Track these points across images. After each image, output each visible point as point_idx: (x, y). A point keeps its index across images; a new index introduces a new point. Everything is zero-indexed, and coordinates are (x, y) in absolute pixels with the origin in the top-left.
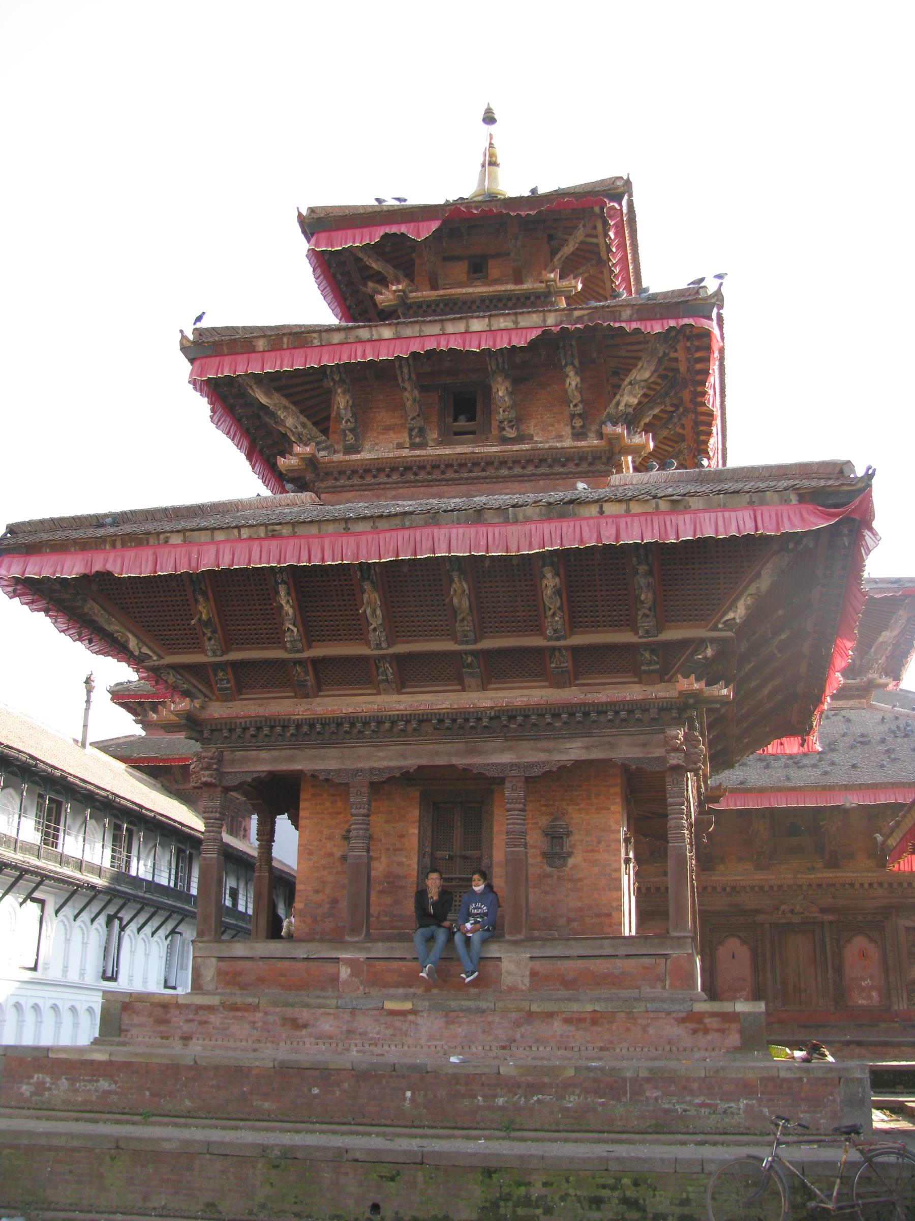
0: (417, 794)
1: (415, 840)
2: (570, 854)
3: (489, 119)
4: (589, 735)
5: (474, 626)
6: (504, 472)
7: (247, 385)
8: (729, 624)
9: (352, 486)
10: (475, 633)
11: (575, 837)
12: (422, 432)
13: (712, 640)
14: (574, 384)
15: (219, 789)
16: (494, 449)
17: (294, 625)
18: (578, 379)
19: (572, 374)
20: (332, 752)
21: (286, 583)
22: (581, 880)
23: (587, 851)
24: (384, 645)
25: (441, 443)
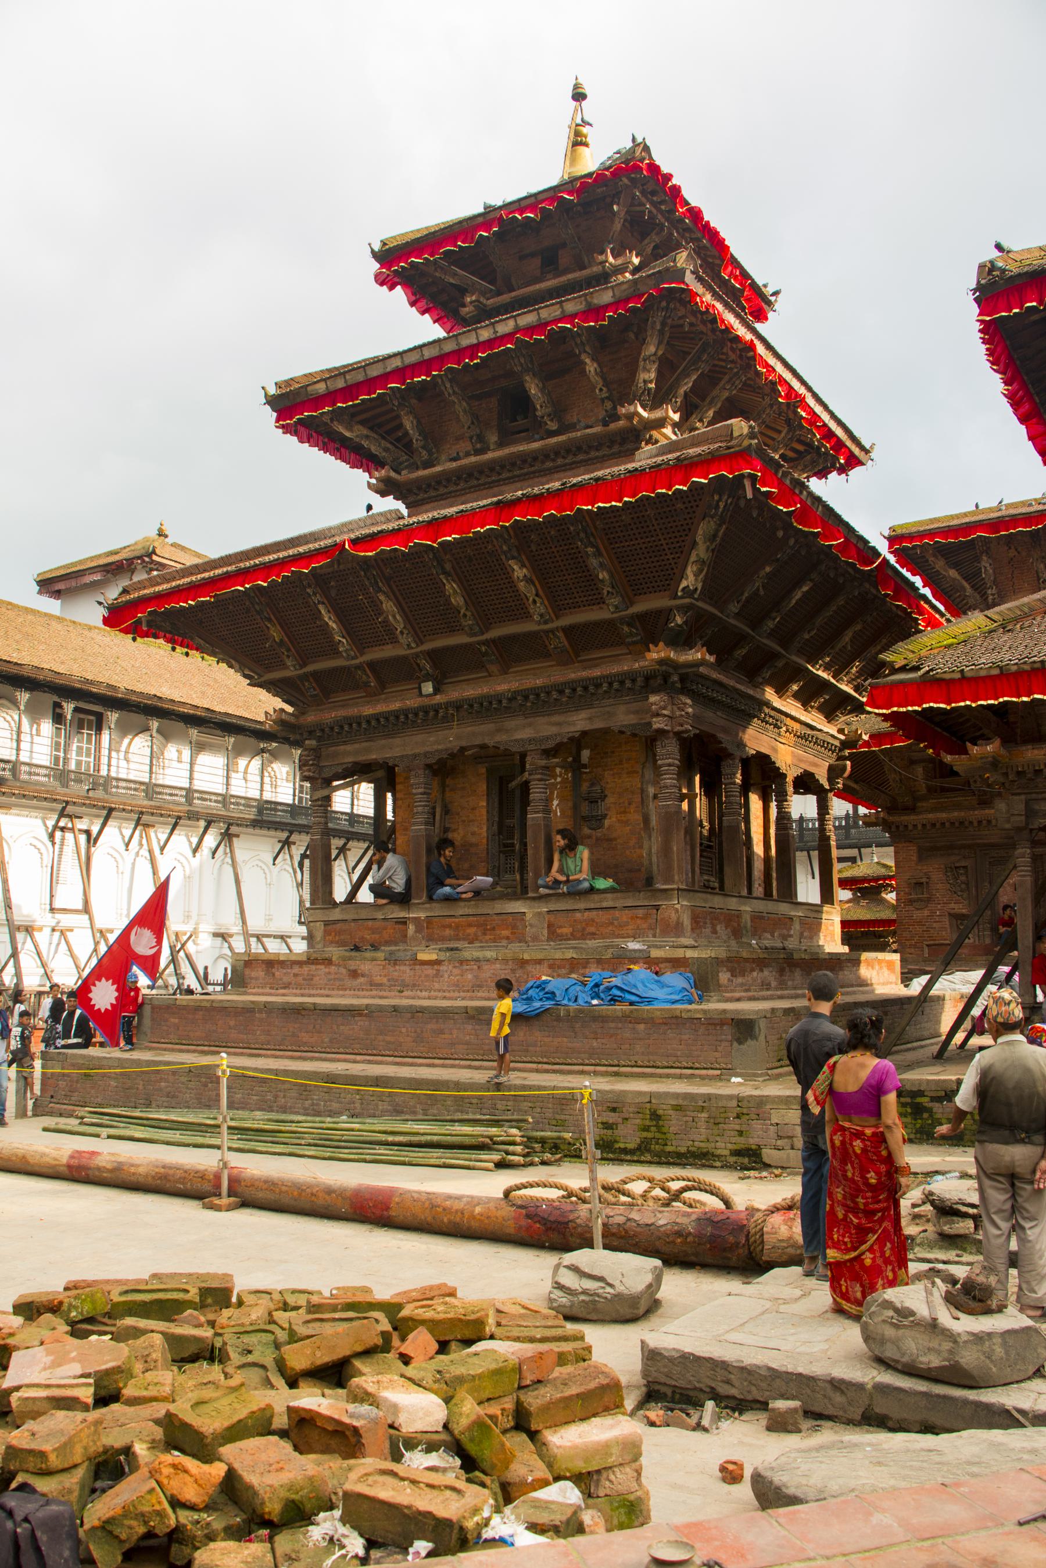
0: (484, 770)
1: (484, 812)
2: (605, 816)
3: (579, 96)
4: (590, 706)
5: (475, 618)
6: (549, 464)
7: (318, 411)
8: (688, 592)
9: (429, 498)
10: (478, 625)
11: (610, 800)
12: (481, 438)
13: (679, 608)
14: (592, 369)
15: (320, 781)
16: (535, 445)
17: (343, 637)
18: (595, 365)
19: (588, 361)
20: (397, 741)
21: (323, 603)
22: (615, 839)
23: (621, 813)
24: (413, 645)
25: (501, 445)
